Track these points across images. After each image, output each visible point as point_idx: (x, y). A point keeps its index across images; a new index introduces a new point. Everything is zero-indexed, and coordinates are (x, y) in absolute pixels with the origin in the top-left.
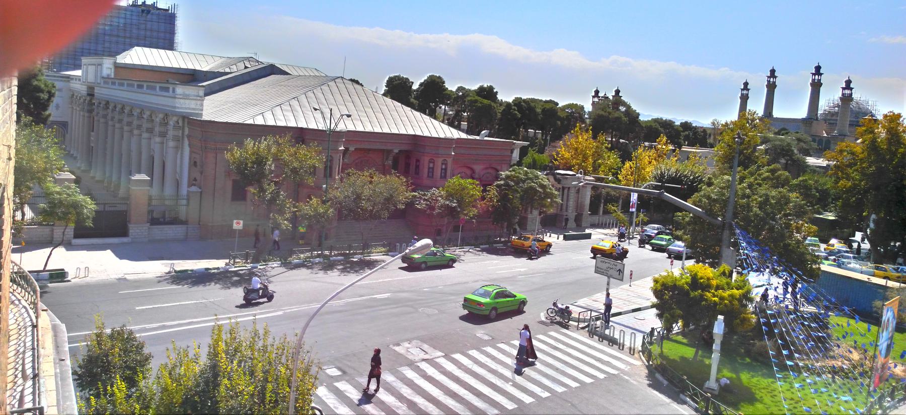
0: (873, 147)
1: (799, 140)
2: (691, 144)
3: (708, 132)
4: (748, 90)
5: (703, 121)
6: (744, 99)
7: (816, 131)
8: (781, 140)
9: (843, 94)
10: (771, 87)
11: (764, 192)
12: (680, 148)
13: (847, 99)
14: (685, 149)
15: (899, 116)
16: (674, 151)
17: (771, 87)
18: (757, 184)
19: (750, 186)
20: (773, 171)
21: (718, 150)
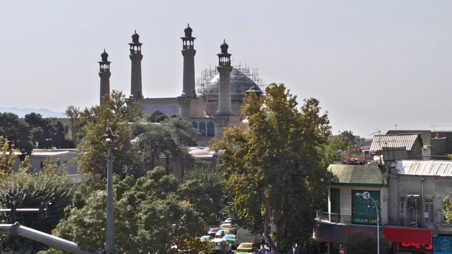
0: (263, 129)
1: (178, 126)
2: (44, 146)
3: (64, 125)
4: (108, 63)
5: (54, 109)
6: (105, 75)
7: (196, 112)
8: (157, 128)
9: (221, 63)
10: (136, 58)
11: (148, 206)
12: (29, 153)
13: (225, 69)
14: (36, 153)
15: (282, 87)
16: (21, 158)
17: (136, 58)
18: (139, 197)
19: (131, 200)
20: (156, 177)
21: (84, 150)
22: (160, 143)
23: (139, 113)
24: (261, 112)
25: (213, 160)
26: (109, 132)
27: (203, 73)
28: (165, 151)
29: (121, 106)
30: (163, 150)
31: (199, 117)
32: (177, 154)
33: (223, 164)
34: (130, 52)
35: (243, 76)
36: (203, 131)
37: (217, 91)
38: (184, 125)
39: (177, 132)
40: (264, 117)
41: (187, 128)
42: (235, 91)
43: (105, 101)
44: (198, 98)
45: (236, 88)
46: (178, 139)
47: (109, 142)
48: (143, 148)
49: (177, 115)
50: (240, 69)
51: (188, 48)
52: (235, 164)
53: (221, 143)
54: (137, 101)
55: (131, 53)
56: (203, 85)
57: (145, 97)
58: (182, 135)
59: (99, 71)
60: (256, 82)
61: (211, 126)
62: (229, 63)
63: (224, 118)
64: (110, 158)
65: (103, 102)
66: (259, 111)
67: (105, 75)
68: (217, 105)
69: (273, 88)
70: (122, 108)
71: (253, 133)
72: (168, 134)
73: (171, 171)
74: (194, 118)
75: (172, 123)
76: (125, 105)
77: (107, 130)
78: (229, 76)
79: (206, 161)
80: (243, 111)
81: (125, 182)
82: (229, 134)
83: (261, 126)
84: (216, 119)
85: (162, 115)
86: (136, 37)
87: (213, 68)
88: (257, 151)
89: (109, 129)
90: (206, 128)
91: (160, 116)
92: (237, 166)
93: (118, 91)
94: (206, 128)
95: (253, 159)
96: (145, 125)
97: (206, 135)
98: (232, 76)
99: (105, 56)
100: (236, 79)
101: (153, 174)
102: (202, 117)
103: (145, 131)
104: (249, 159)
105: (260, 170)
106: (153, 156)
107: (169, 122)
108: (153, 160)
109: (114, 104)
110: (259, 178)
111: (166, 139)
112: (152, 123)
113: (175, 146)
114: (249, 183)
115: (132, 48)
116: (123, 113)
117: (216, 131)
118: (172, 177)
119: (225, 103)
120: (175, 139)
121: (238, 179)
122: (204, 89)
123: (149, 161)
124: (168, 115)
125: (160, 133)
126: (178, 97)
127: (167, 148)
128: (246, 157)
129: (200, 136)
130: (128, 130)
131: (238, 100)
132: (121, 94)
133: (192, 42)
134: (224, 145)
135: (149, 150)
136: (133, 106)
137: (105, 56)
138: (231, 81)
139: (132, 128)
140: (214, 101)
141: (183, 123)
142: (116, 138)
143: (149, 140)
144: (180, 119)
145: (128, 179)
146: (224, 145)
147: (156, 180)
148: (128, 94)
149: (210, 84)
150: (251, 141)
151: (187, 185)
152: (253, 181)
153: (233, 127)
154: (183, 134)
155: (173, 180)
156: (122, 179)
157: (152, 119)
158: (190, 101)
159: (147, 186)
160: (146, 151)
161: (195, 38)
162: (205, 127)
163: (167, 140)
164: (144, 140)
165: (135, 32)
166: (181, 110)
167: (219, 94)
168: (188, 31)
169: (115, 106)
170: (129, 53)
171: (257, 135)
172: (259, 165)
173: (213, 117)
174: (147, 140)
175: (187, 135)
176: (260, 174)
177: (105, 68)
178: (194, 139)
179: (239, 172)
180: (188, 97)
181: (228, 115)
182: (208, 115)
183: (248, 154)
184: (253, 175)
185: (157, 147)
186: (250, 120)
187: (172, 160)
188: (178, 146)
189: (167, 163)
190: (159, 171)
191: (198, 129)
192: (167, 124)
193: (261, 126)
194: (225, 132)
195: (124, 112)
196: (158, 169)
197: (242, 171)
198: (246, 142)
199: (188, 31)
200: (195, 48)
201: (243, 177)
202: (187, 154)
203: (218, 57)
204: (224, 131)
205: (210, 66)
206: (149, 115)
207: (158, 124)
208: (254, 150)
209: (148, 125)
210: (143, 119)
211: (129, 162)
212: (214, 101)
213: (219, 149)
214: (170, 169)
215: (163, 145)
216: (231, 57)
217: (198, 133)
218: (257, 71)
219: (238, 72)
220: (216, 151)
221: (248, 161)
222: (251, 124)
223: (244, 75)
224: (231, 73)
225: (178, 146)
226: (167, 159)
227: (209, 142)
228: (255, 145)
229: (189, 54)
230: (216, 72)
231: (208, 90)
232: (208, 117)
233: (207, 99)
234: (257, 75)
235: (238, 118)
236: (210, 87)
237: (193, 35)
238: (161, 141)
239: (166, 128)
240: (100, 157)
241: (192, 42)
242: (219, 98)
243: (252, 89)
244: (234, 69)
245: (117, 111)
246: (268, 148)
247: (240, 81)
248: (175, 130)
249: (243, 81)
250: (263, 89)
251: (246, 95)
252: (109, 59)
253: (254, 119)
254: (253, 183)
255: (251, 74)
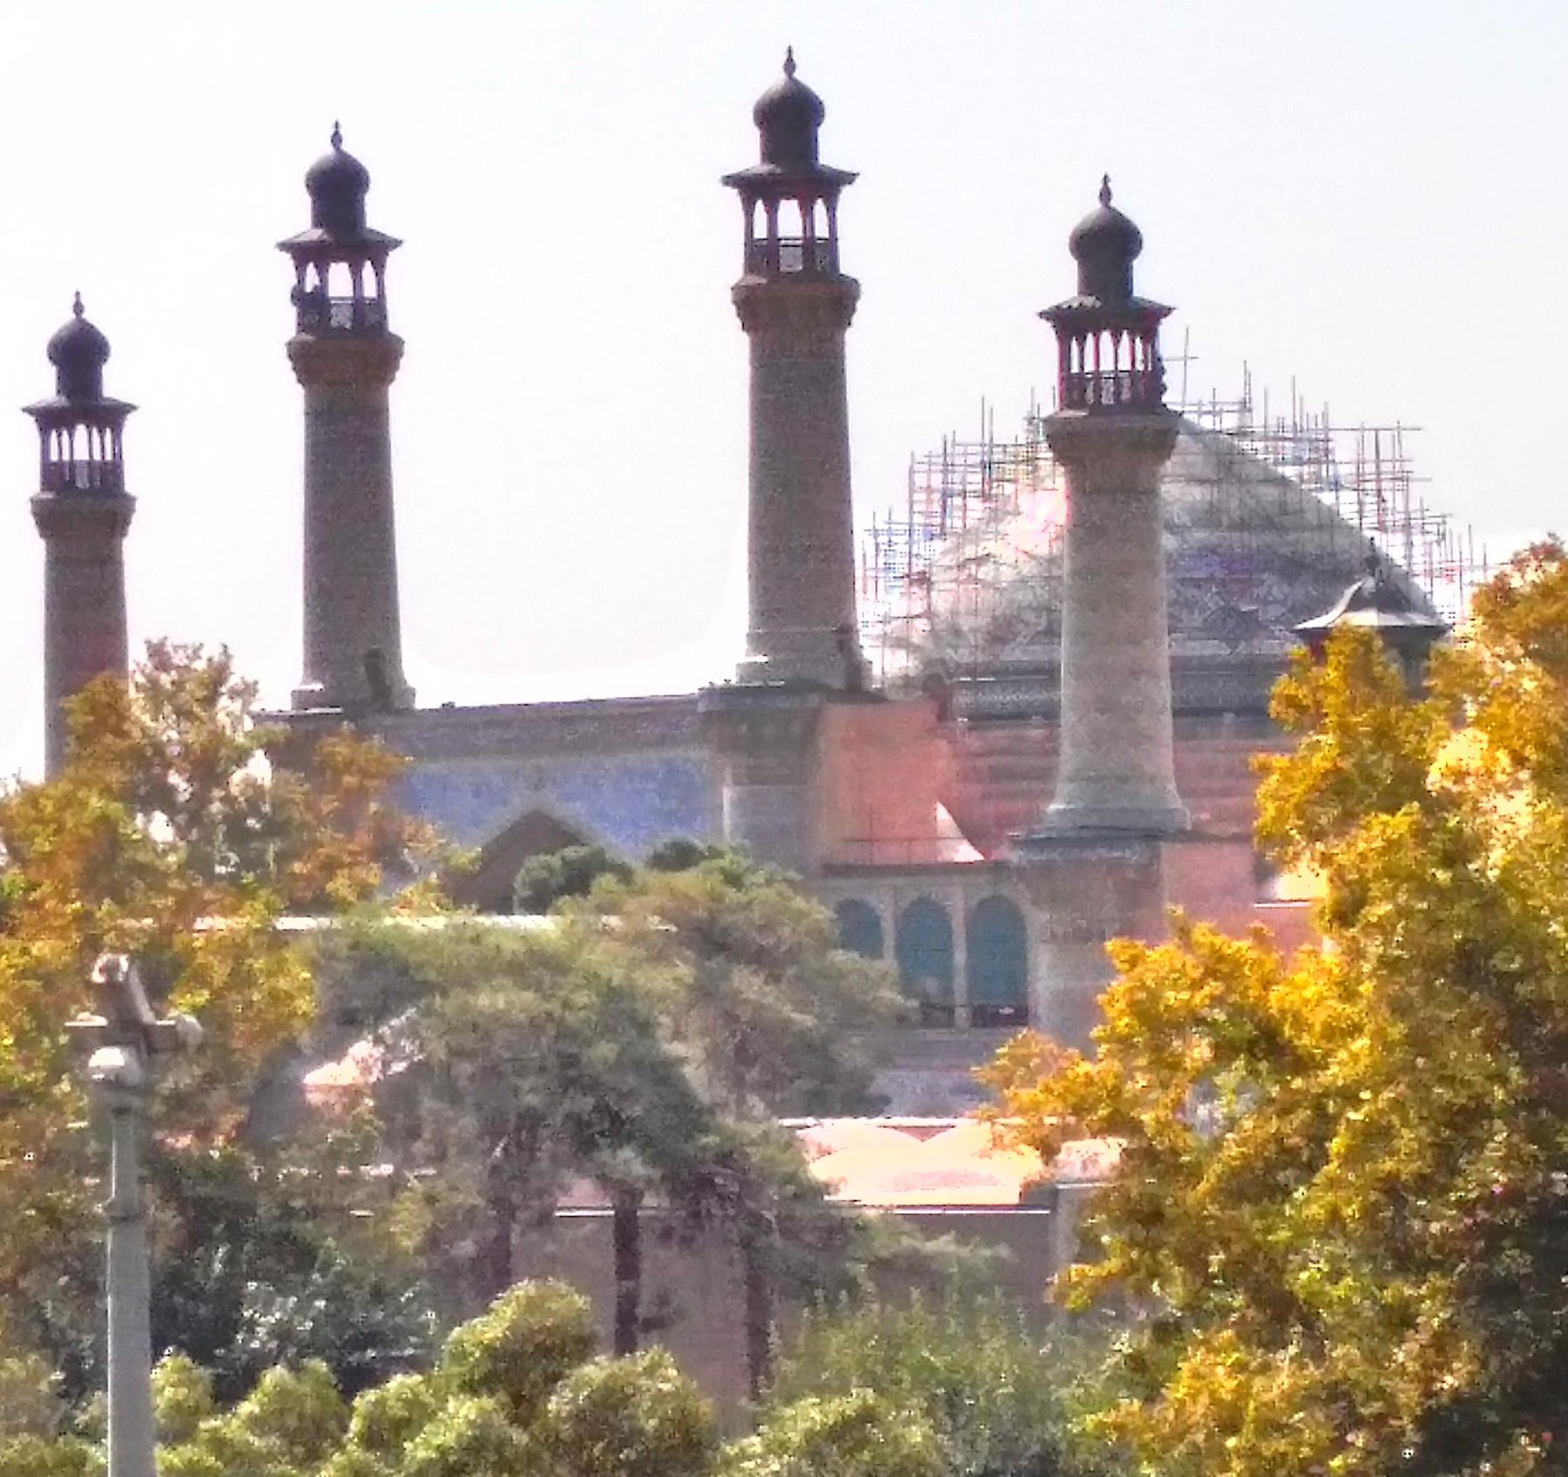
1: (710, 939)
6: (84, 519)
8: (534, 966)
9: (1073, 387)
10: (345, 363)
13: (1112, 433)
17: (345, 363)
20: (517, 1373)
22: (566, 1099)
23: (380, 833)
24: (1436, 805)
25: (1027, 1227)
26: (112, 994)
27: (920, 480)
28: (604, 1155)
29: (222, 780)
30: (585, 1140)
31: (893, 854)
32: (706, 1183)
33: (1113, 1264)
34: (291, 313)
35: (1270, 493)
36: (931, 985)
37: (1051, 633)
38: (766, 927)
39: (704, 992)
40: (1458, 852)
41: (793, 955)
42: (1209, 630)
43: (85, 738)
44: (878, 698)
45: (1211, 599)
46: (712, 1054)
47: (115, 1082)
48: (414, 1133)
49: (700, 844)
50: (1241, 433)
51: (792, 262)
52: (1216, 1259)
53: (1089, 1080)
54: (361, 734)
55: (302, 327)
56: (924, 580)
57: (426, 700)
58: (745, 1015)
59: (31, 483)
60: (1391, 546)
61: (1001, 937)
62: (1151, 380)
63: (1115, 867)
64: (125, 1218)
65: (72, 746)
66: (1422, 795)
67: (84, 519)
68: (1050, 750)
69: (1546, 592)
70: (228, 800)
71: (1366, 988)
72: (622, 1011)
73: (650, 1325)
74: (848, 870)
75: (664, 914)
76: (259, 768)
77: (97, 978)
78: (1153, 493)
79: (962, 1240)
80: (1270, 799)
81: (255, 1423)
82: (1155, 996)
83: (1436, 924)
84: (1047, 869)
85: (571, 852)
86: (338, 187)
87: (1012, 429)
88: (1407, 1138)
89: (110, 970)
90: (960, 957)
91: (555, 861)
92: (1235, 1273)
93: (196, 655)
94: (960, 957)
95: (1369, 1211)
96: (428, 941)
97: (962, 1014)
98: (1178, 490)
99: (79, 353)
100: (1210, 516)
101: (490, 1351)
102: (920, 854)
103: (426, 988)
104: (1334, 1214)
105: (1433, 1315)
106: (497, 1202)
107: (631, 904)
108: (503, 1239)
109: (168, 765)
110: (1426, 1382)
111: (605, 1050)
112: (485, 921)
113: (689, 1115)
114: (1343, 1429)
115: (312, 279)
116: (238, 835)
117: (1046, 976)
118: (650, 1371)
119: (1115, 742)
120: (690, 1057)
121: (1243, 1392)
122: (929, 614)
123: (466, 1248)
124: (628, 849)
125: (554, 1007)
126: (711, 693)
127: (619, 1130)
128: (1308, 1203)
129: (902, 1019)
130: (283, 984)
131: (1229, 705)
132: (217, 676)
133: (820, 207)
134: (1115, 1093)
135: (466, 1150)
136: (321, 773)
137: (79, 353)
138: (1169, 542)
139: (314, 966)
140: (1019, 716)
141: (756, 915)
142: (175, 1041)
143: (465, 1068)
144: (734, 880)
145: (282, 1392)
146: (1115, 1093)
147: (517, 1399)
148: (276, 667)
149: (986, 572)
150: (1347, 1062)
151: (795, 1437)
152: (1377, 1406)
153: (1184, 933)
154: (759, 1007)
155: (660, 1397)
156: (227, 1393)
157: (483, 888)
158: (813, 721)
159: (442, 1451)
160: (439, 1158)
161: (850, 178)
162: (947, 950)
163: (619, 1065)
164: (419, 1071)
165: (336, 139)
166: (738, 803)
167: (1064, 652)
168: (790, 118)
169: (174, 778)
170: (285, 323)
171: (1400, 1009)
172: (1427, 1265)
173: (1014, 856)
174: (447, 1068)
175: (787, 1010)
176: (1442, 1344)
177: (81, 454)
178: (853, 1053)
179: (1247, 1335)
180: (799, 687)
181: (1152, 836)
182: (972, 834)
183: (1332, 1168)
184: (1375, 1358)
185: (532, 1120)
186: (1338, 879)
187: (666, 1234)
188: (711, 1111)
189: (628, 1264)
190: (534, 1322)
191: (888, 963)
192: (614, 921)
193: (1436, 924)
194: (1119, 985)
195: (250, 834)
196: (531, 1306)
197: (1280, 1316)
198: (1304, 1064)
199: (790, 118)
200: (848, 265)
201: (1285, 1374)
202: (791, 1178)
203: (1047, 332)
204: (1112, 972)
205: (986, 414)
206: (466, 854)
207: (544, 926)
208: (1376, 1135)
209: (458, 935)
210: (409, 890)
211: (291, 1257)
212: (1019, 716)
213: (1068, 1133)
214: (642, 1311)
215: (589, 1102)
216: (1166, 328)
217: (890, 995)
218: (1398, 441)
219: (1226, 461)
220: (1048, 1151)
221: (1325, 1236)
222: (1345, 914)
223: (1283, 481)
224: (1168, 466)
225: (711, 1111)
226: (626, 1230)
227: (979, 1073)
228: (1388, 1094)
229: (797, 313)
230: (1031, 461)
231: (965, 624)
232: (966, 853)
233: (963, 699)
234: (1403, 478)
235: (1237, 861)
236: (988, 595)
237: (831, 150)
238: (569, 1073)
239: (607, 960)
240: (51, 1215)
241: (820, 207)
242: (1066, 692)
243: (1357, 604)
244: (1196, 433)
245: (191, 817)
246: (1508, 1114)
247: (1254, 540)
248: (685, 971)
249: (1269, 538)
250: (1452, 603)
251: (1297, 649)
252: (114, 383)
253: (1374, 865)
254: (1381, 1419)
255: (1346, 471)
